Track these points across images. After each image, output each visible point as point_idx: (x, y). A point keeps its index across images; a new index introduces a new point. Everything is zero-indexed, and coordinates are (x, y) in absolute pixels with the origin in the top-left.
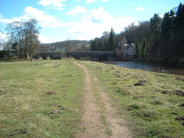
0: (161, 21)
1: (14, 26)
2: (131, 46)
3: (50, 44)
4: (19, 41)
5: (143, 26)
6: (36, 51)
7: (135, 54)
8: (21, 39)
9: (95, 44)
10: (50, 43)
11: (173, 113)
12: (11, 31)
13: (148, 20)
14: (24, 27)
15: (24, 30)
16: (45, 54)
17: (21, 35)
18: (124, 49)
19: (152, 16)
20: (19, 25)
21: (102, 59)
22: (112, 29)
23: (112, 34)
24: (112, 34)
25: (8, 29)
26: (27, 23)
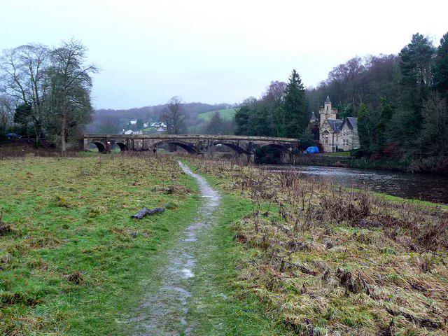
0: (434, 56)
1: (22, 57)
2: (346, 125)
3: (123, 111)
4: (32, 101)
5: (381, 67)
6: (92, 129)
7: (92, 129)
8: (40, 96)
9: (248, 117)
10: (126, 109)
11: (30, 303)
12: (12, 72)
13: (396, 52)
14: (48, 63)
15: (50, 71)
16: (105, 139)
17: (40, 83)
18: (326, 132)
19: (406, 41)
20: (34, 56)
21: (270, 157)
22: (295, 75)
23: (295, 86)
24: (295, 86)
25: (4, 66)
26: (56, 52)
